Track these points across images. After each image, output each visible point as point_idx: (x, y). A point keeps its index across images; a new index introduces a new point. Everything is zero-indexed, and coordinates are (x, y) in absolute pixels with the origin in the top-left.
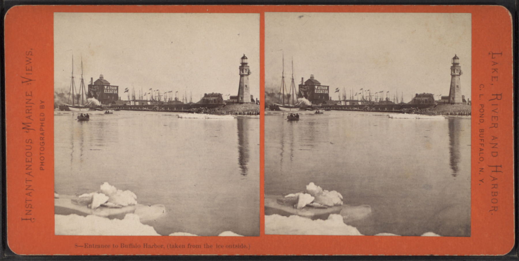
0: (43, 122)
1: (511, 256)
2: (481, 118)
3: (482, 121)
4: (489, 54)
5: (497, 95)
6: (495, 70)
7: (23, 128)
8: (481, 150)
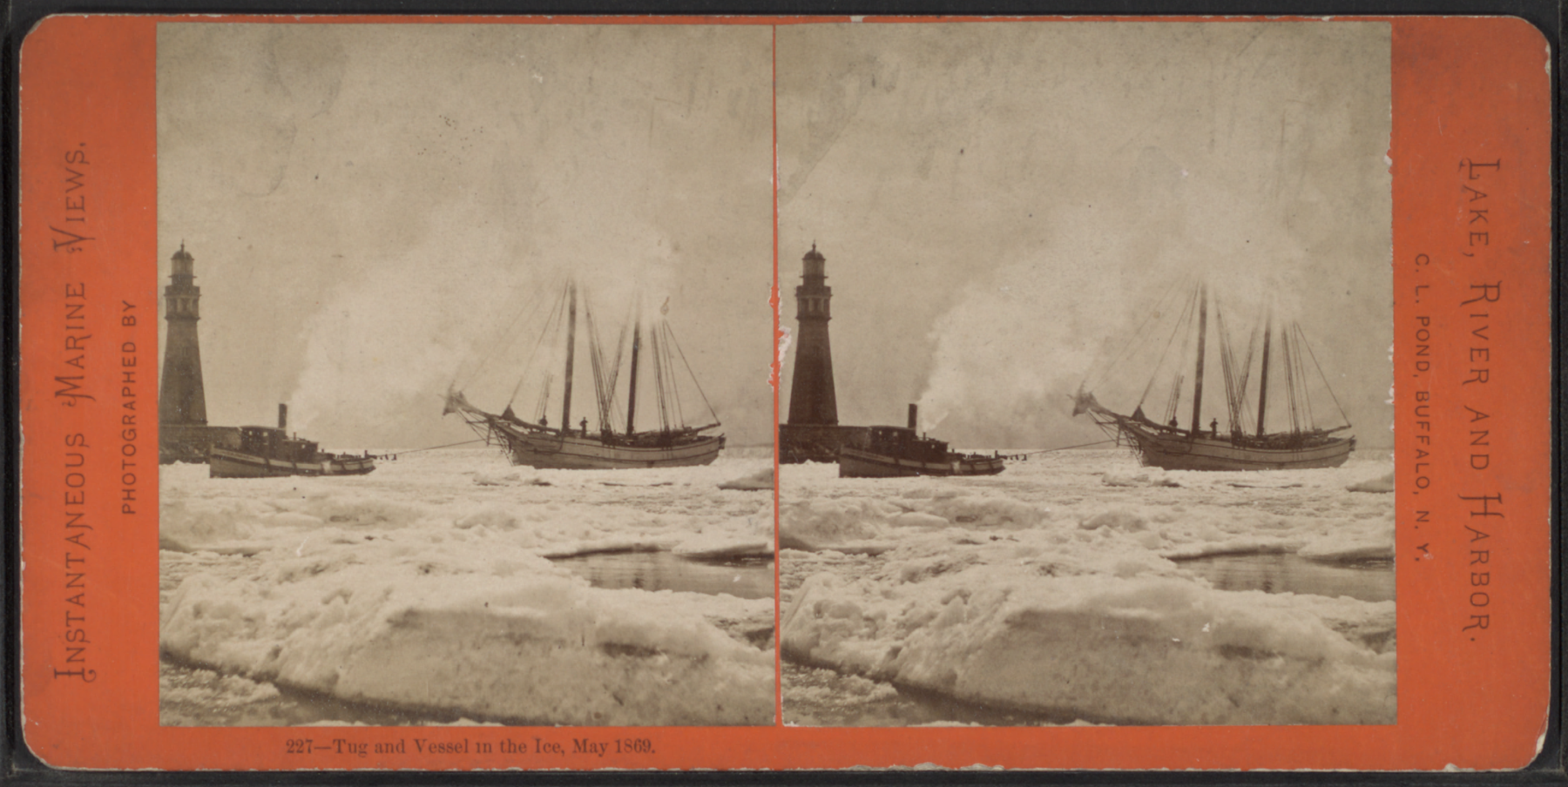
1: (1545, 770)
2: (1421, 358)
3: (1423, 366)
4: (1461, 165)
5: (1485, 287)
6: (1479, 214)
7: (58, 393)
8: (1422, 454)
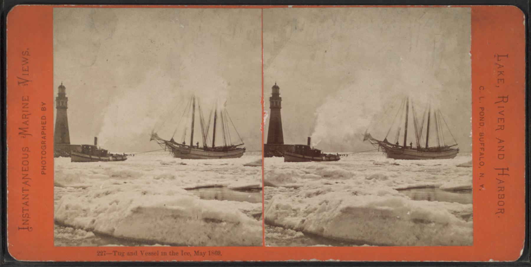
0: (44, 125)
1: (523, 261)
4: (495, 56)
5: (503, 97)
7: (20, 133)
8: (481, 154)
